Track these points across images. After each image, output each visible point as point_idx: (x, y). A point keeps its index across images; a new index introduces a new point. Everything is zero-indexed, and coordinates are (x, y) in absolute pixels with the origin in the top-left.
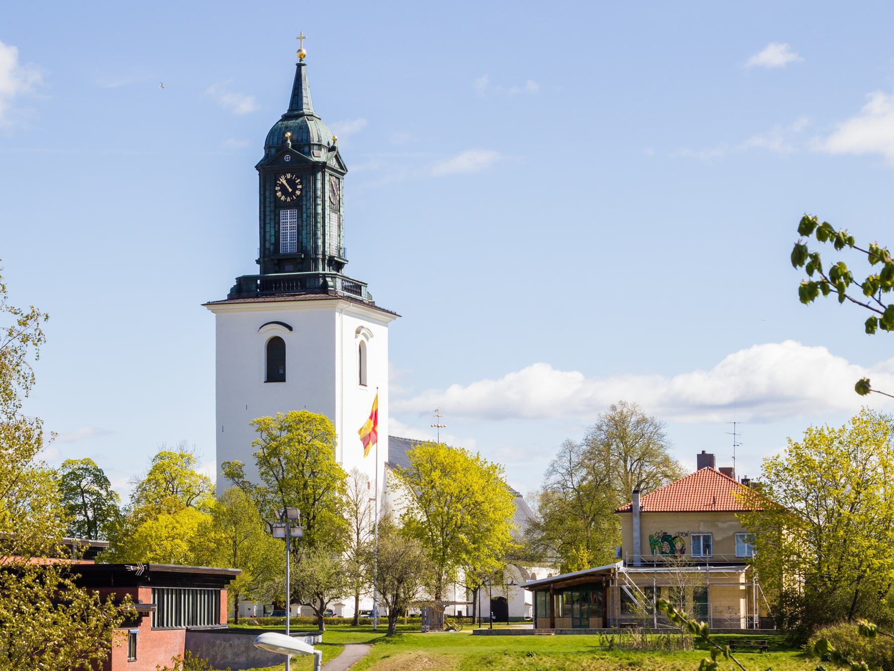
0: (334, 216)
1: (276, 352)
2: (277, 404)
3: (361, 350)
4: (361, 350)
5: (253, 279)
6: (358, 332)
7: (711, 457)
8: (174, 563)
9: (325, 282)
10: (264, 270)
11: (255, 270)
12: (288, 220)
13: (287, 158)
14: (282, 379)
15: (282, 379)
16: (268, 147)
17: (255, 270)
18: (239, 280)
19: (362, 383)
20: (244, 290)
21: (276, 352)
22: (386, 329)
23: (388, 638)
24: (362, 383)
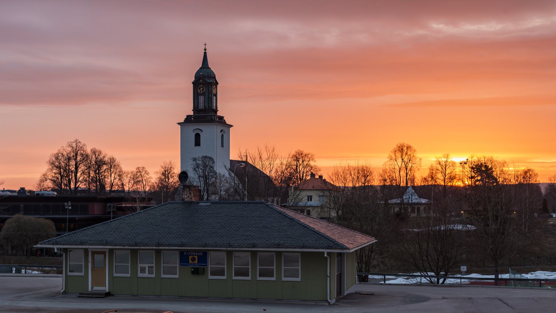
0: (215, 97)
1: (198, 136)
2: (199, 152)
3: (222, 135)
4: (222, 135)
5: (191, 116)
6: (221, 131)
7: (193, 273)
8: (72, 211)
9: (212, 118)
10: (194, 113)
11: (192, 113)
12: (201, 99)
13: (201, 81)
14: (200, 145)
15: (200, 145)
16: (195, 77)
17: (192, 113)
18: (187, 116)
19: (222, 146)
20: (188, 120)
21: (198, 136)
22: (231, 159)
23: (337, 303)
24: (222, 146)
